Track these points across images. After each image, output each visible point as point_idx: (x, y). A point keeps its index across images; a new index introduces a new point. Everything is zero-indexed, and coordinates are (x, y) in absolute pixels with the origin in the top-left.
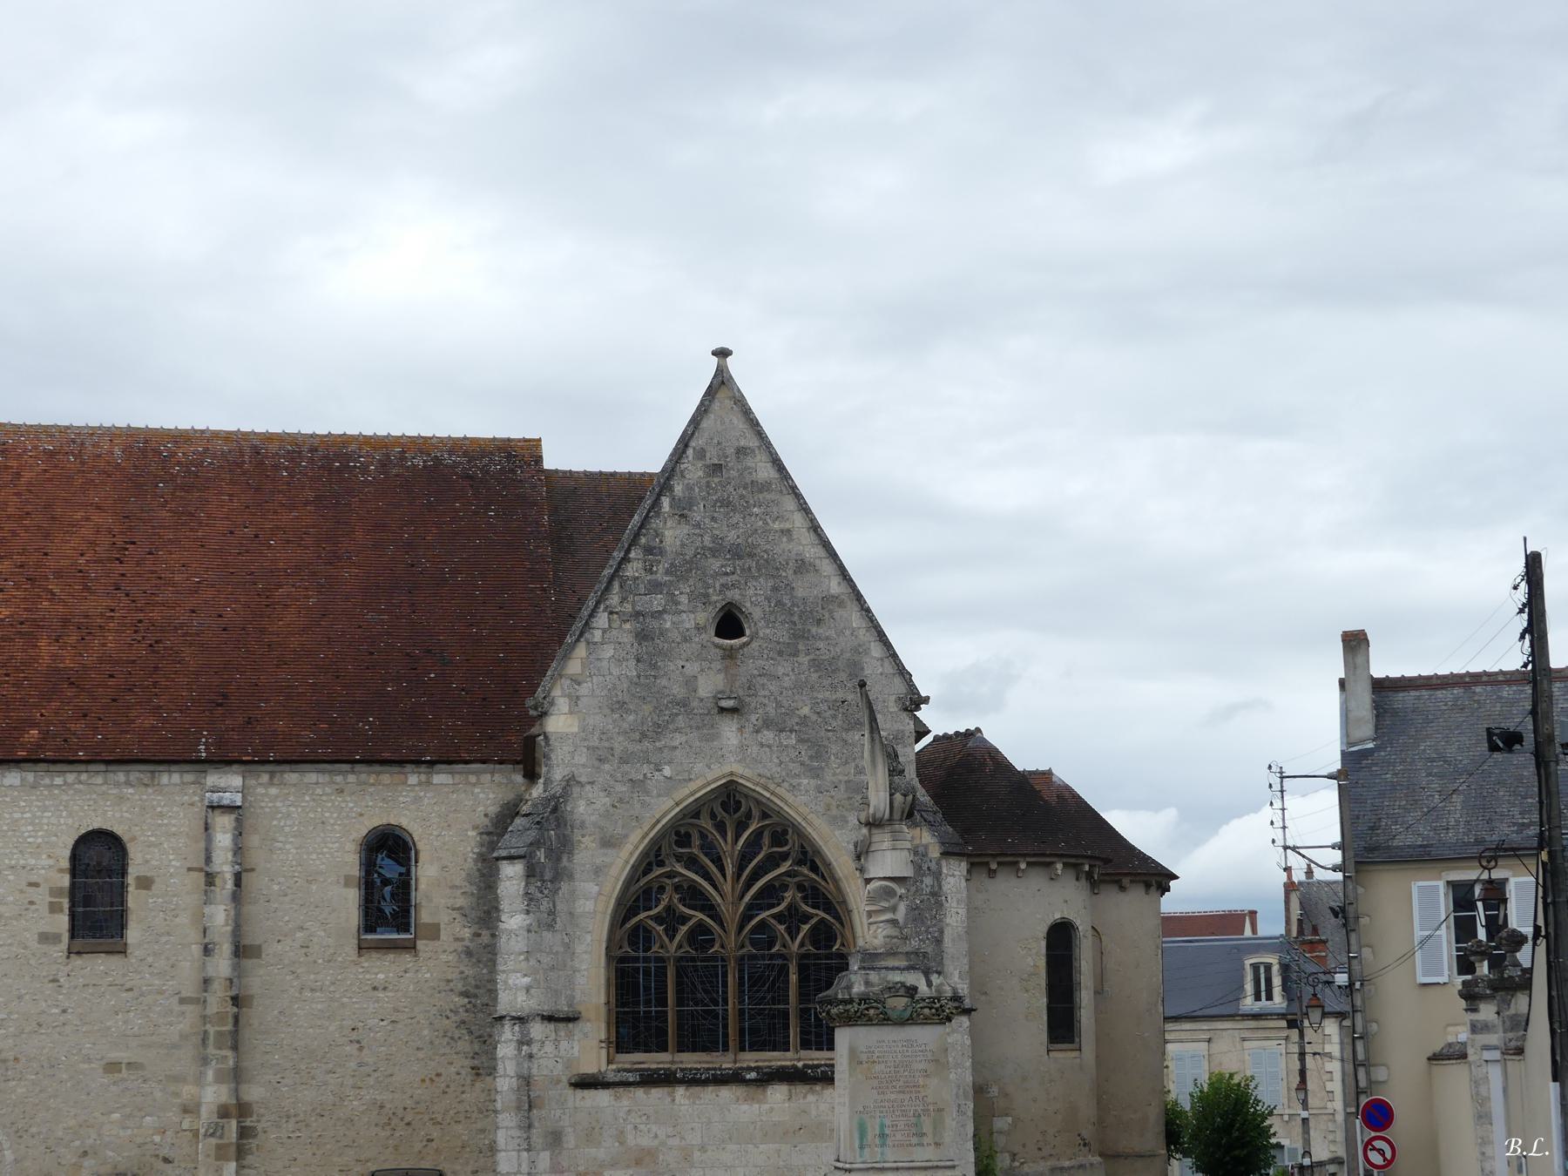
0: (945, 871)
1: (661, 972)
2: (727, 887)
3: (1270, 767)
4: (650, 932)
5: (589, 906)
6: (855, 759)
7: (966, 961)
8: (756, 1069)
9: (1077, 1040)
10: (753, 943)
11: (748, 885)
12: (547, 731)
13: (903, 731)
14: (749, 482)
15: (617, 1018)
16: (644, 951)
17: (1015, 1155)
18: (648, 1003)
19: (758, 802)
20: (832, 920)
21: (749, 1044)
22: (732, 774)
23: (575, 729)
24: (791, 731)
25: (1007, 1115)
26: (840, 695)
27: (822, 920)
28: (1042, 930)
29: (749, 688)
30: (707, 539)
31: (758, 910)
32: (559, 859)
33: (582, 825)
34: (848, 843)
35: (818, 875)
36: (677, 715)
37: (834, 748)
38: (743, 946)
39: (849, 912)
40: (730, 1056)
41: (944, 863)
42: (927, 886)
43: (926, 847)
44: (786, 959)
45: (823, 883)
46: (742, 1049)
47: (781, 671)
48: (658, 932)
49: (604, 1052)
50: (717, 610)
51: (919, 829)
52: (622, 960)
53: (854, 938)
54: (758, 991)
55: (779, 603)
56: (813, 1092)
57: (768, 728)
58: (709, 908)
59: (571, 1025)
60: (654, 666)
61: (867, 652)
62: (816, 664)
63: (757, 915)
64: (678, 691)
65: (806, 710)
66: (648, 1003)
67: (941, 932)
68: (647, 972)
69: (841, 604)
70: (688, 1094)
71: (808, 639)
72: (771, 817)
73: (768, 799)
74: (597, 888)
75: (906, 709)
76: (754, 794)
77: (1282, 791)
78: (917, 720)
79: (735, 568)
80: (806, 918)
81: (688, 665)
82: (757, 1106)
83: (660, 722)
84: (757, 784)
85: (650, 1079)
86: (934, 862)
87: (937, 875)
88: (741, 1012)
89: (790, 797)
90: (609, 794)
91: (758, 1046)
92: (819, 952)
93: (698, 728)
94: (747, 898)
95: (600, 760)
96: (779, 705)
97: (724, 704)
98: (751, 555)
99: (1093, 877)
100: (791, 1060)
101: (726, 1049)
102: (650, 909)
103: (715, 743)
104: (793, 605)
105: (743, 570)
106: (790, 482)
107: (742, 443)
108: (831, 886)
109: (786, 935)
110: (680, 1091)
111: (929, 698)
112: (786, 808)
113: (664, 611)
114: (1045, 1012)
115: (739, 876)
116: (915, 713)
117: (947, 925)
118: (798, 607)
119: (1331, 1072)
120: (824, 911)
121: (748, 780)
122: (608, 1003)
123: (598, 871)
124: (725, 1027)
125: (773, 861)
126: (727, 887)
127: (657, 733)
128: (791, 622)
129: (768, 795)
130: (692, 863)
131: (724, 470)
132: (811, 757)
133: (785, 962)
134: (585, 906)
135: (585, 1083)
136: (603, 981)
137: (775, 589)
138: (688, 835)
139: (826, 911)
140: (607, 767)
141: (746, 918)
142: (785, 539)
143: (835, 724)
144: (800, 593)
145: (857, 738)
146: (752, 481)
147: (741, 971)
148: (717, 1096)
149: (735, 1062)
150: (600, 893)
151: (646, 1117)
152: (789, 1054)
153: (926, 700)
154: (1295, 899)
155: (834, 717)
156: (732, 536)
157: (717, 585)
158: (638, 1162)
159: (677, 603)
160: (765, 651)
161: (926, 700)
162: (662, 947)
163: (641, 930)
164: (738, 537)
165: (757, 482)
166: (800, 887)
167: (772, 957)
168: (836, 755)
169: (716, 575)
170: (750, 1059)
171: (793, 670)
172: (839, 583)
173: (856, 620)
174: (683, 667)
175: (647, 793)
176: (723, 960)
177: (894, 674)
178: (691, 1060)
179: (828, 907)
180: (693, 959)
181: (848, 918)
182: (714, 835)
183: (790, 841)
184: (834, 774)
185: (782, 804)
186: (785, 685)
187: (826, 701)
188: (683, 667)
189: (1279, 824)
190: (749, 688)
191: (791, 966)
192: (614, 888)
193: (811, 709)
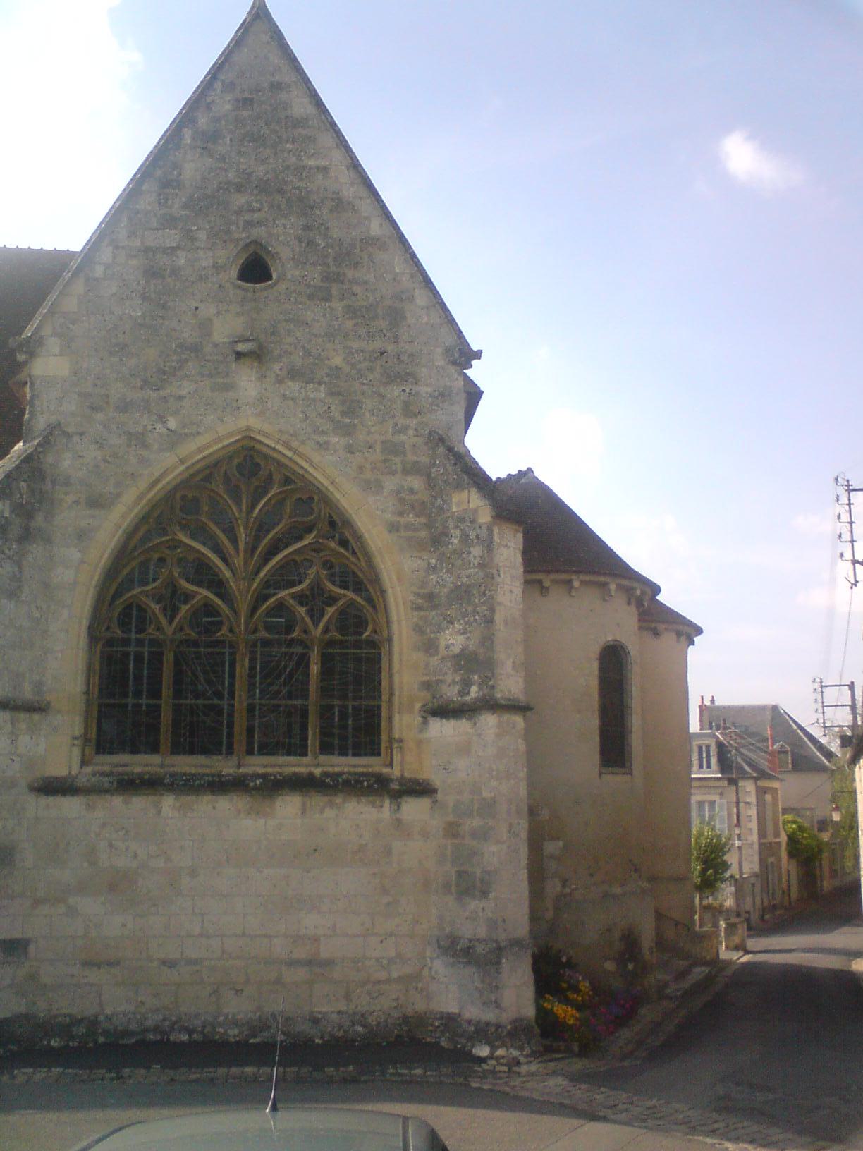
0: (496, 538)
1: (157, 657)
2: (239, 561)
3: (836, 480)
4: (145, 611)
5: (69, 575)
6: (393, 417)
7: (520, 649)
8: (264, 776)
9: (627, 764)
10: (268, 627)
11: (266, 560)
12: (32, 374)
13: (451, 387)
14: (283, 117)
15: (99, 711)
16: (137, 633)
17: (567, 880)
18: (138, 694)
19: (280, 465)
20: (363, 603)
21: (259, 746)
22: (248, 429)
23: (66, 373)
24: (320, 383)
25: (558, 839)
26: (378, 345)
27: (352, 603)
28: (595, 649)
29: (273, 334)
30: (231, 175)
31: (275, 589)
32: (30, 515)
33: (67, 482)
34: (383, 511)
35: (347, 550)
36: (186, 360)
37: (369, 404)
38: (255, 631)
39: (383, 592)
40: (234, 760)
41: (496, 530)
42: (475, 558)
43: (475, 511)
44: (306, 647)
45: (353, 559)
46: (250, 752)
47: (309, 316)
48: (153, 612)
49: (76, 752)
50: (239, 248)
51: (467, 491)
52: (110, 643)
53: (388, 623)
54: (271, 684)
55: (311, 243)
56: (331, 804)
57: (292, 378)
58: (217, 585)
59: (36, 717)
60: (164, 307)
61: (411, 299)
62: (351, 311)
63: (274, 594)
64: (188, 335)
65: (338, 361)
66: (138, 694)
67: (492, 610)
68: (139, 659)
69: (383, 247)
70: (178, 805)
71: (342, 282)
72: (295, 482)
73: (290, 459)
74: (79, 555)
75: (454, 363)
76: (275, 455)
77: (849, 504)
78: (467, 378)
79: (262, 204)
80: (333, 600)
81: (201, 306)
82: (262, 821)
83: (166, 369)
84: (278, 441)
85: (129, 785)
86: (484, 528)
87: (489, 546)
88: (251, 709)
89: (316, 458)
90: (101, 447)
91: (268, 749)
92: (346, 638)
93: (210, 376)
94: (262, 574)
95: (93, 409)
96: (308, 353)
97: (241, 347)
98: (281, 191)
99: (643, 605)
100: (307, 766)
101: (230, 751)
102: (147, 584)
103: (230, 393)
104: (327, 246)
105: (271, 207)
106: (329, 119)
107: (277, 78)
108: (363, 564)
109: (308, 620)
110: (168, 802)
111: (480, 352)
112: (311, 470)
113: (178, 247)
114: (597, 732)
115: (253, 550)
116: (465, 371)
117: (499, 604)
118: (332, 248)
119: (751, 816)
120: (354, 591)
121: (267, 436)
122: (87, 693)
123: (82, 536)
124: (231, 725)
125: (296, 533)
126: (239, 561)
127: (162, 381)
128: (325, 264)
129: (289, 454)
130: (200, 532)
131: (255, 105)
132: (343, 414)
133: (307, 650)
134: (64, 575)
135: (52, 787)
136: (81, 664)
137: (307, 228)
138: (196, 501)
139: (356, 591)
140: (99, 416)
141: (261, 598)
142: (320, 177)
143: (371, 377)
144: (335, 234)
145: (396, 393)
146: (287, 117)
147: (253, 660)
148: (214, 808)
149: (239, 766)
150: (82, 562)
151: (124, 831)
152: (305, 760)
153: (478, 355)
154: (706, 714)
155: (371, 369)
156: (261, 171)
157: (241, 224)
158: (112, 888)
159: (193, 239)
160: (294, 295)
161: (478, 355)
162: (158, 629)
163: (135, 609)
164: (267, 172)
165: (292, 117)
166: (328, 565)
167: (291, 643)
168: (372, 412)
169: (239, 212)
170: (258, 765)
171: (324, 315)
172: (381, 225)
173: (399, 266)
174: (197, 308)
175: (145, 446)
176: (231, 646)
177: (442, 324)
178: (187, 764)
179: (359, 587)
180: (195, 644)
181: (381, 600)
182: (225, 500)
183: (316, 509)
184: (369, 433)
185: (306, 466)
186: (314, 331)
187: (362, 351)
188: (197, 308)
189: (847, 537)
190: (273, 334)
191: (312, 655)
192: (101, 558)
193: (344, 359)
